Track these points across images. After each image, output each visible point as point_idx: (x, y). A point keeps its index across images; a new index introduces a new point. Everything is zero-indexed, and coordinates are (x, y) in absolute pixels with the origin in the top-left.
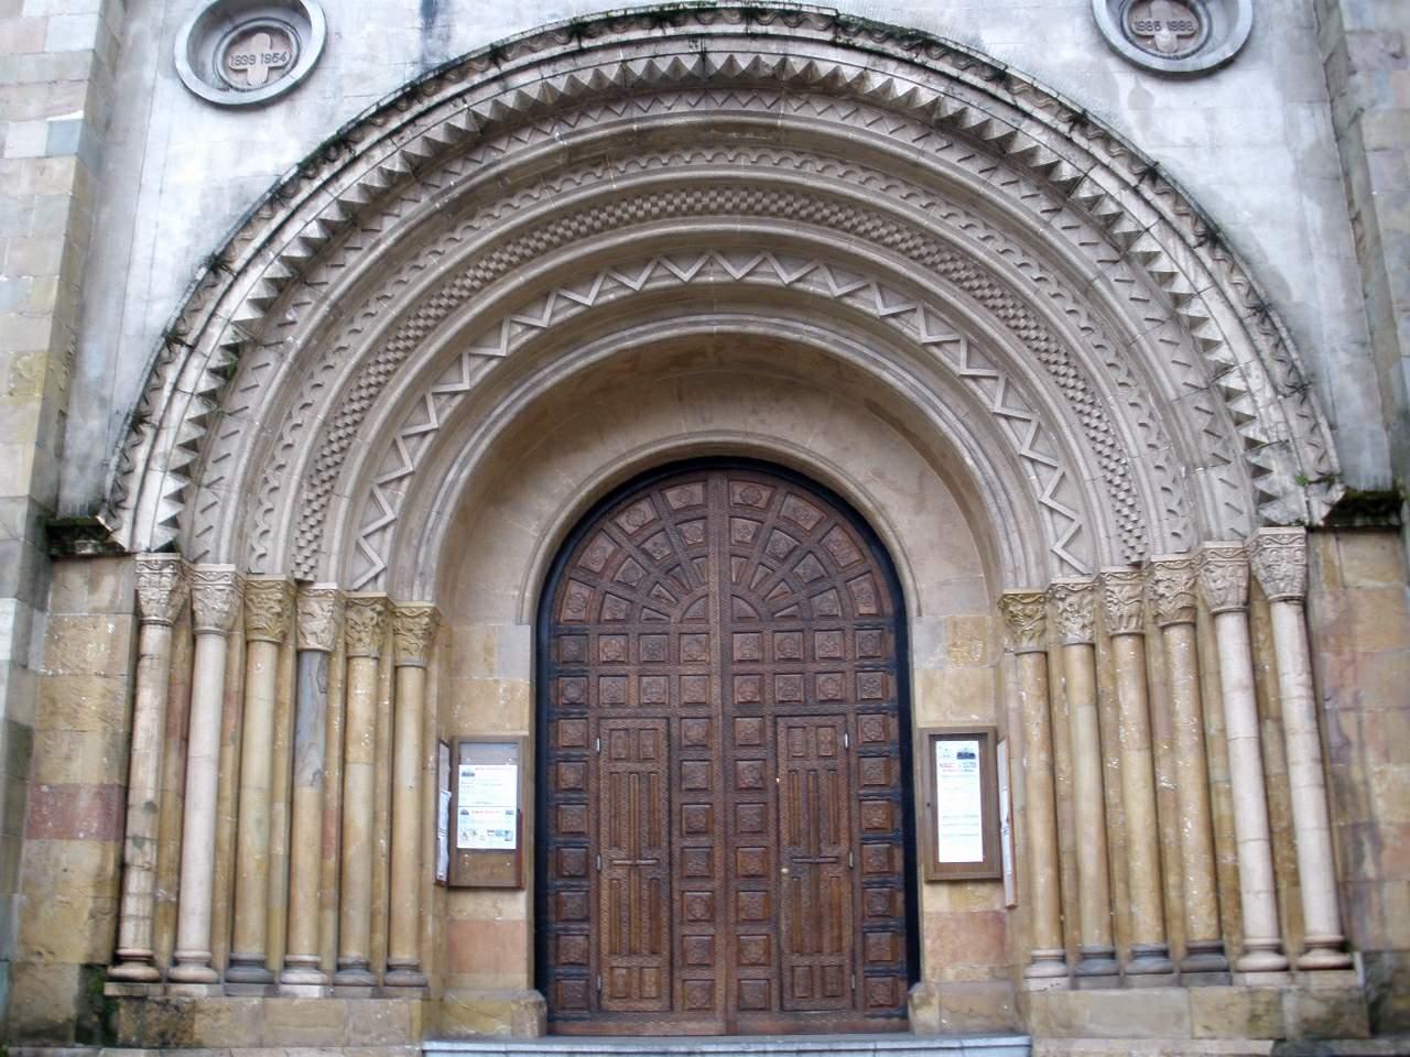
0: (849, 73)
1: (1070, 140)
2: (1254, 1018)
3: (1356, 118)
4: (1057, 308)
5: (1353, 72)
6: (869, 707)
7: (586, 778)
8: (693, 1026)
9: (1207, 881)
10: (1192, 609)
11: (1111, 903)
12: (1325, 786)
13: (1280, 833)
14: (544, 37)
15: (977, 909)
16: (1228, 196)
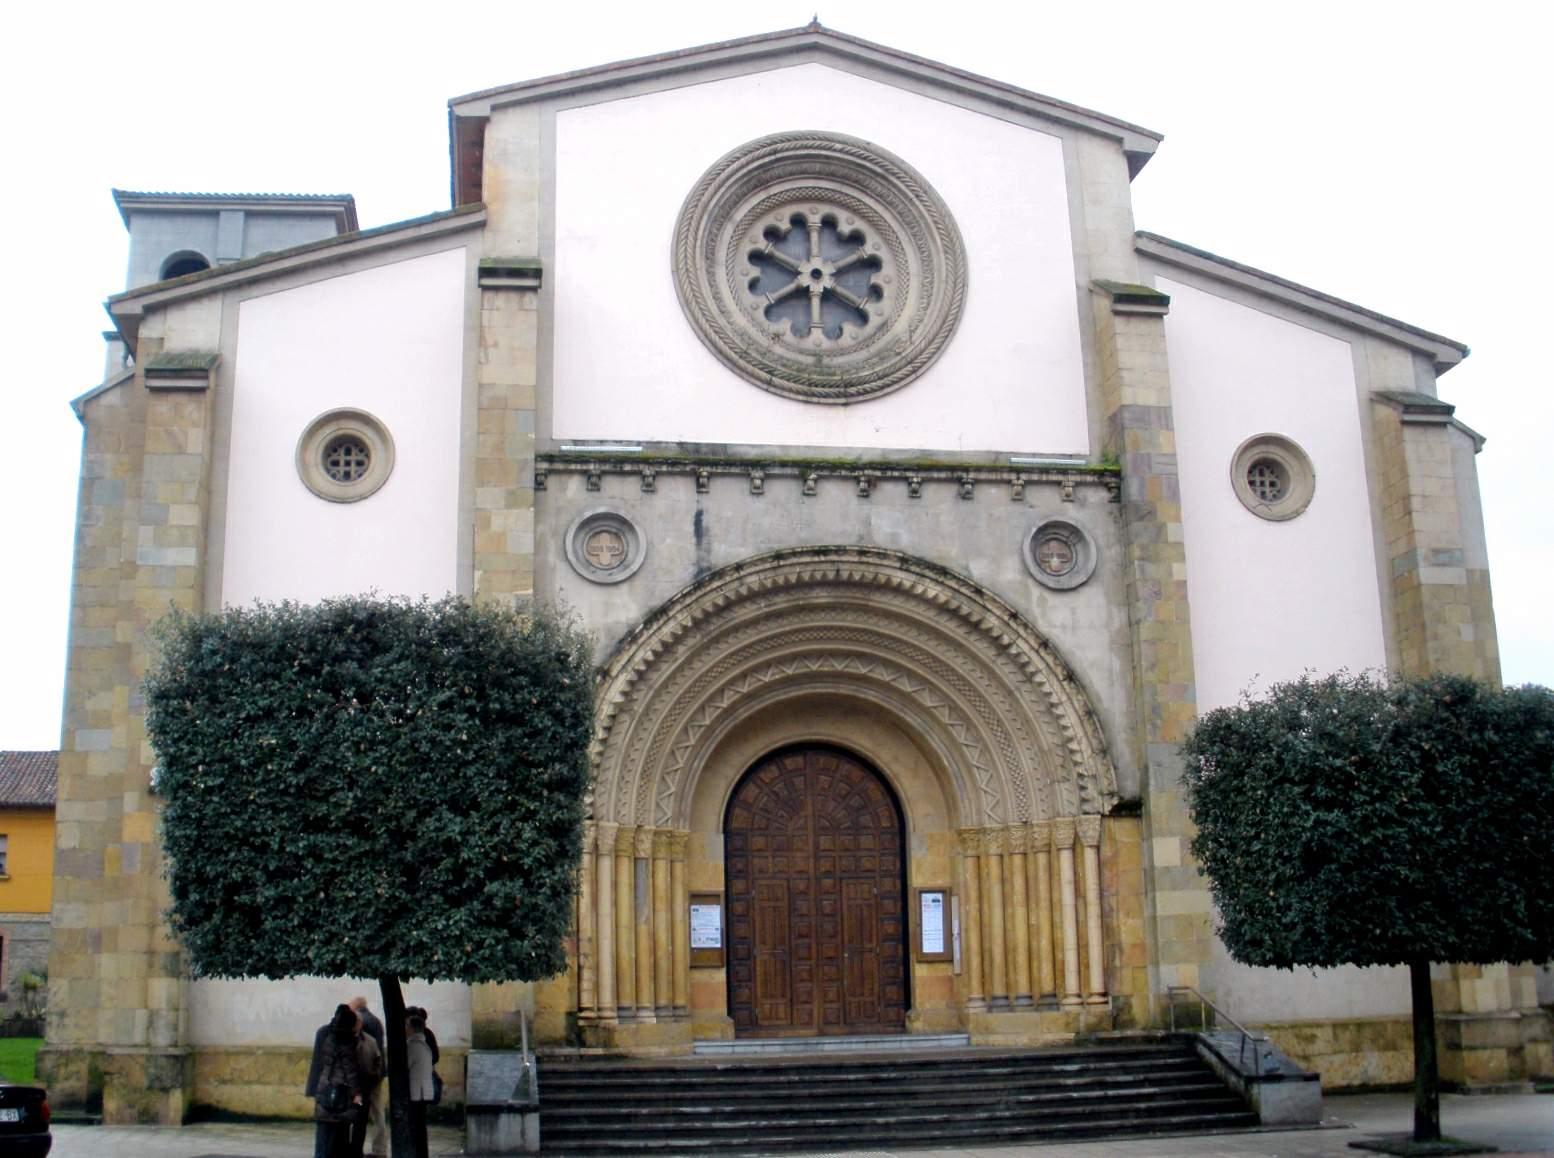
0: (907, 584)
1: (1008, 625)
2: (1067, 1024)
3: (1138, 622)
4: (997, 701)
5: (1138, 600)
6: (886, 874)
7: (748, 909)
8: (802, 1032)
9: (1050, 966)
10: (1049, 845)
11: (1007, 975)
12: (1102, 927)
13: (1082, 947)
14: (763, 560)
15: (940, 974)
16: (1078, 653)
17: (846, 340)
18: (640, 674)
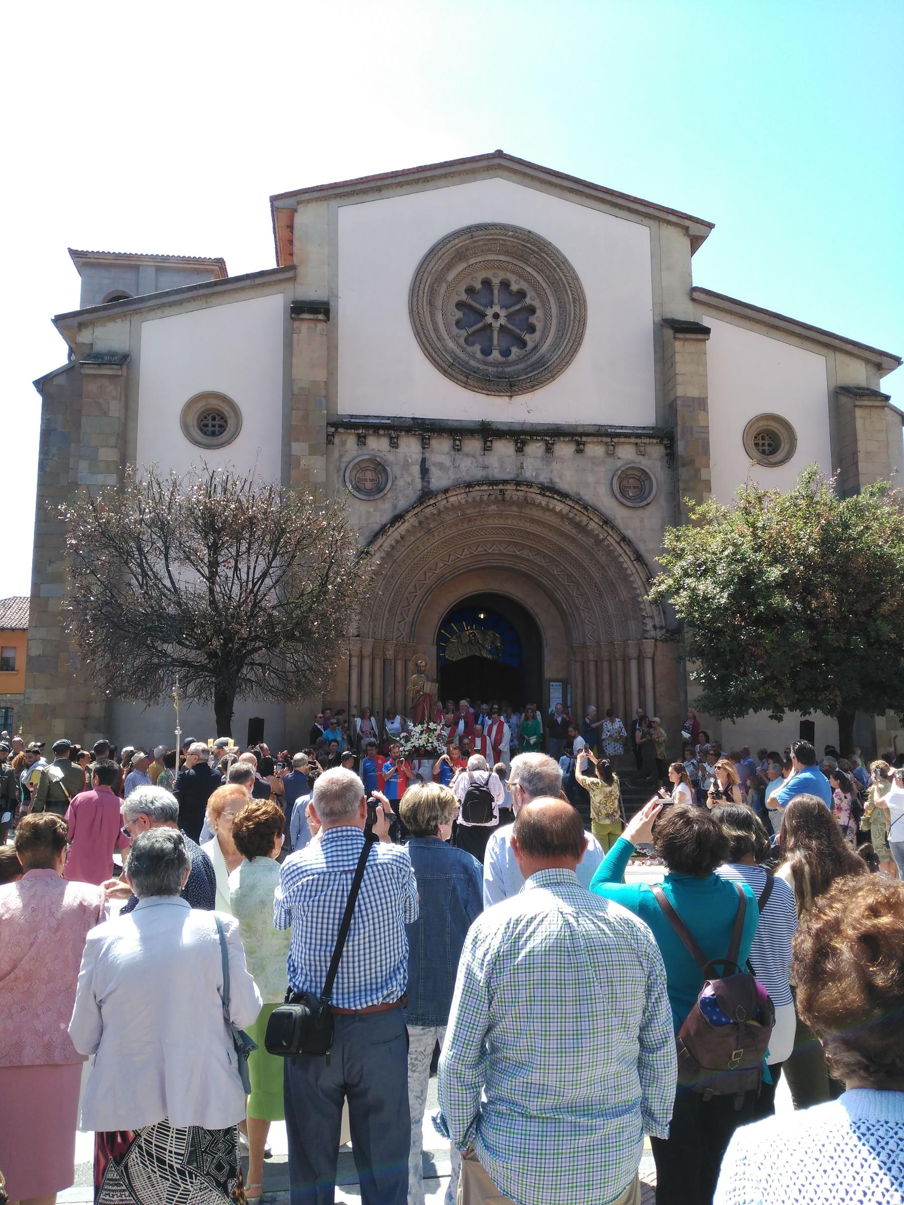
9: (529, 169)
17: (513, 357)
18: (440, 512)
